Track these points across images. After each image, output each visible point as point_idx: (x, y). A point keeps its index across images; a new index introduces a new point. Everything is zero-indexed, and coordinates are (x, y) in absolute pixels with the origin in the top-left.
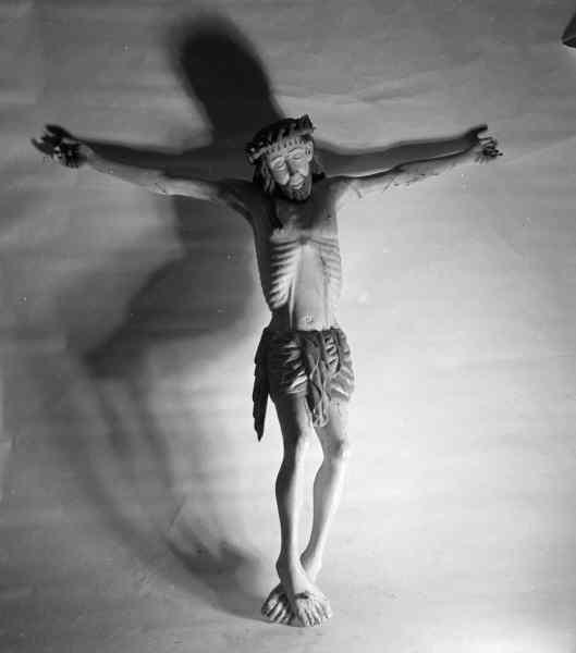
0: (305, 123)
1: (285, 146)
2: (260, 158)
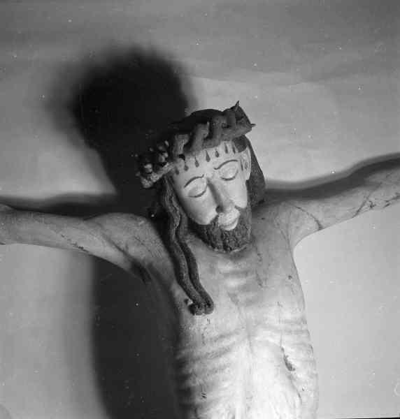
0: (236, 118)
1: (208, 159)
2: (161, 180)
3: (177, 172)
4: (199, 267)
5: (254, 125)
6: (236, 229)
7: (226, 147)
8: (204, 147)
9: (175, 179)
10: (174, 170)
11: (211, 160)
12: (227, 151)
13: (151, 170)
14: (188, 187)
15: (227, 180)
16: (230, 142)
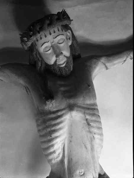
2: (32, 44)
3: (37, 40)
4: (64, 111)
5: (72, 20)
6: (66, 66)
7: (58, 28)
8: (48, 28)
9: (37, 44)
10: (36, 40)
11: (52, 34)
12: (59, 30)
13: (26, 40)
14: (42, 47)
15: (60, 43)
16: (60, 26)
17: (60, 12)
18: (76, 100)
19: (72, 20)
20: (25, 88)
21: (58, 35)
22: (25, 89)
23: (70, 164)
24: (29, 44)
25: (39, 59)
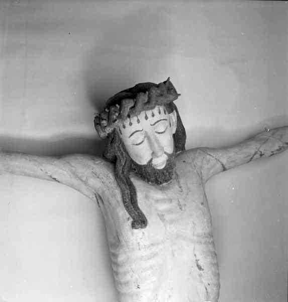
3: (124, 127)
5: (180, 95)
12: (160, 113)
17: (158, 84)
18: (136, 181)
19: (180, 95)
20: (96, 197)
21: (159, 119)
22: (95, 198)
23: (111, 240)
24: (109, 130)
25: (122, 154)
